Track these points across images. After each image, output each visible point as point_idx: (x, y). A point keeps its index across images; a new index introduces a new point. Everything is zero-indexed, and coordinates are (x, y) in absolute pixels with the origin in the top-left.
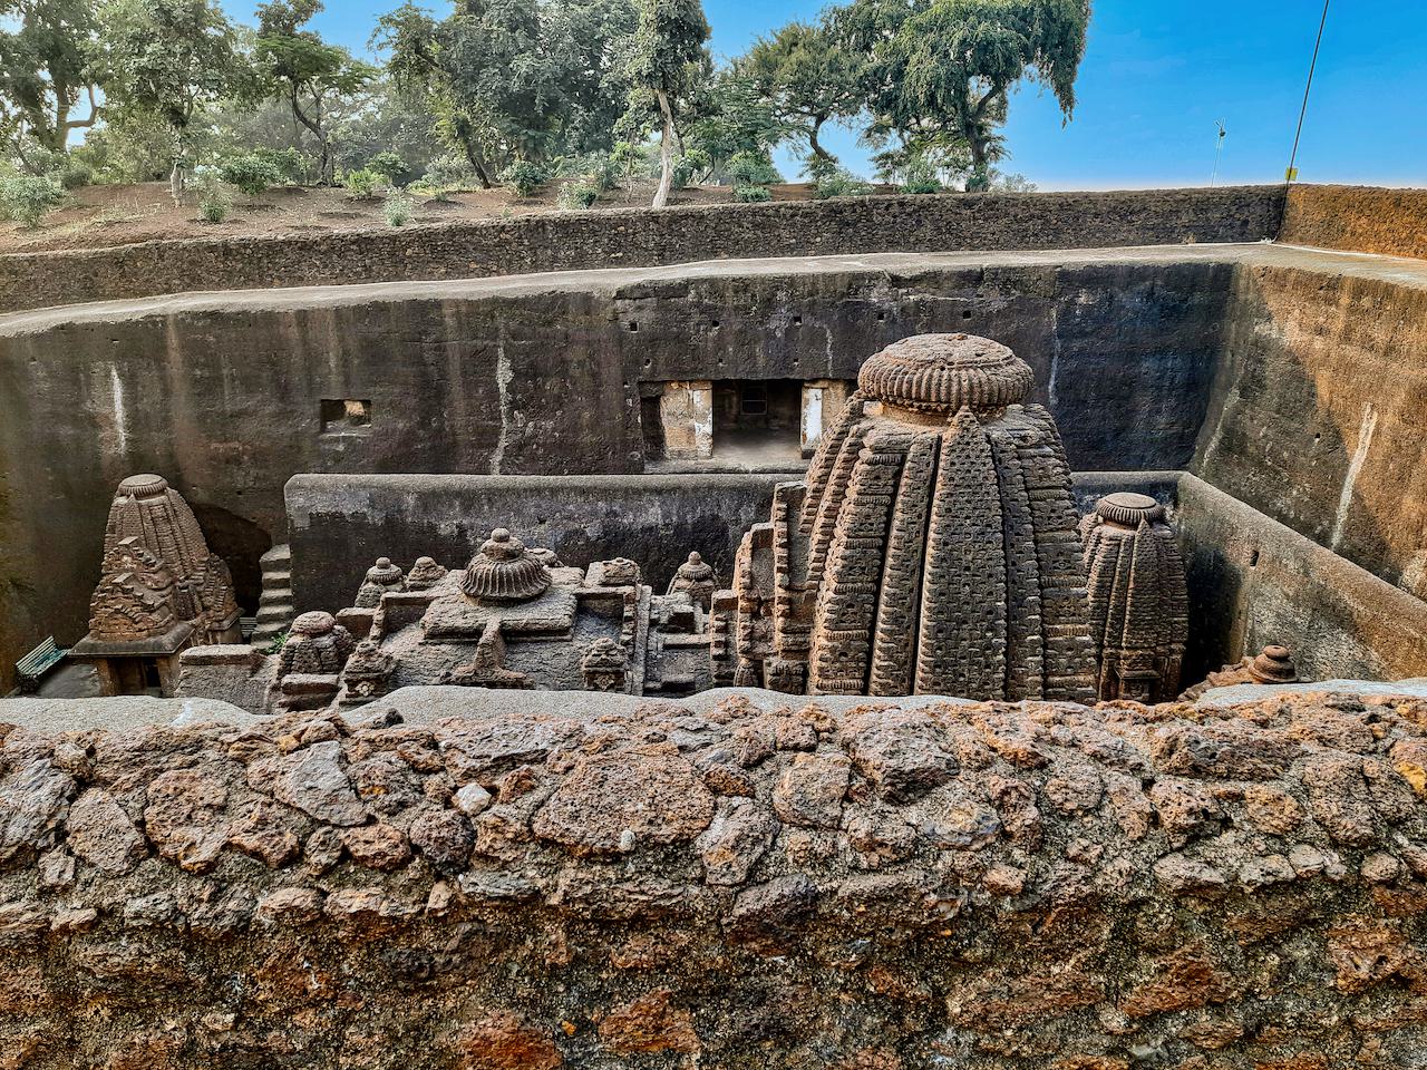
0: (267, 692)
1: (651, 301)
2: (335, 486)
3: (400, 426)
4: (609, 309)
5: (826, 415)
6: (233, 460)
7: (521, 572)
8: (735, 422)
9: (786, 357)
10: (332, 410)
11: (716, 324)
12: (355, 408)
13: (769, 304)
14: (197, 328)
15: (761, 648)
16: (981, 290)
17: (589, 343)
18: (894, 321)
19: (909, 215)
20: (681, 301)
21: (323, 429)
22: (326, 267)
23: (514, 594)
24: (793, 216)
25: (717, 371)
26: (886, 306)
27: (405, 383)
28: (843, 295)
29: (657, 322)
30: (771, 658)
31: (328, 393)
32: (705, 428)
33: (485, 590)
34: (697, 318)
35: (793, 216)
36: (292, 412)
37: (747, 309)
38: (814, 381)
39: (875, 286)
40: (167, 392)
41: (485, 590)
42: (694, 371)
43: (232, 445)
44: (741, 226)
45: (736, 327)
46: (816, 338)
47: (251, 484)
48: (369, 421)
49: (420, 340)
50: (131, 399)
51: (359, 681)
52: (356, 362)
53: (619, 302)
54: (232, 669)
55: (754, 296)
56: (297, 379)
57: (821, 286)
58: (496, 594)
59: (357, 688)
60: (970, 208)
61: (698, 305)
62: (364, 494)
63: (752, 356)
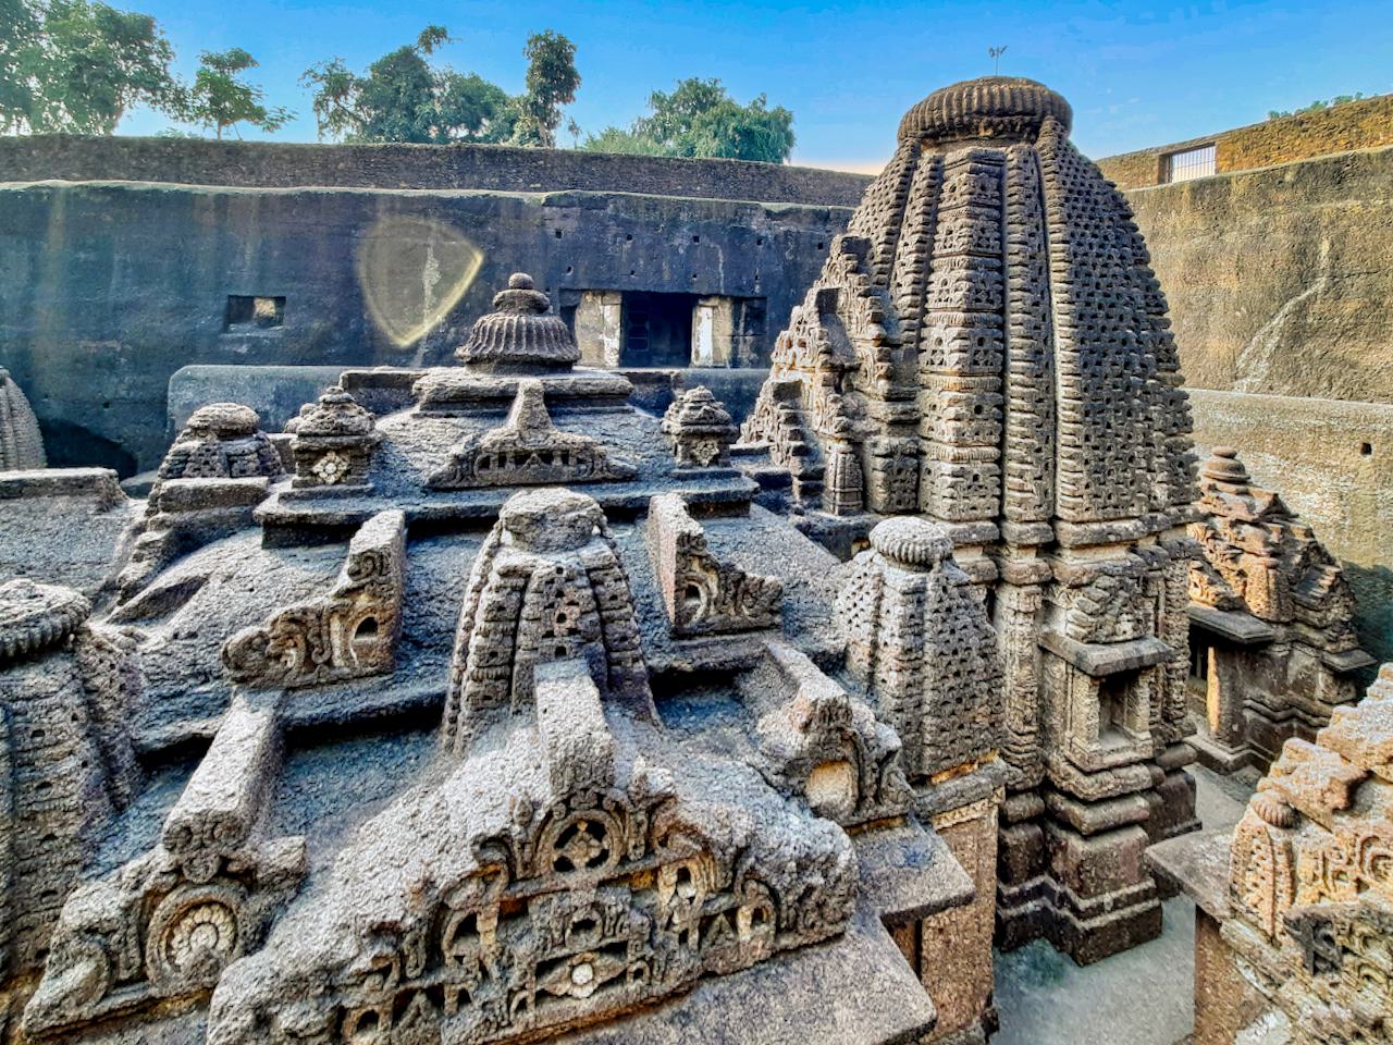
0: (123, 537)
1: (576, 210)
2: (235, 377)
3: (316, 325)
4: (538, 214)
6: (109, 365)
9: (688, 273)
10: (239, 309)
11: (629, 238)
12: (266, 308)
13: (674, 224)
14: (93, 204)
15: (859, 426)
16: (828, 227)
17: (516, 247)
20: (601, 213)
21: (226, 329)
22: (252, 173)
23: (546, 354)
25: (630, 282)
27: (326, 279)
29: (580, 231)
30: (875, 438)
31: (238, 287)
32: (613, 343)
33: (506, 347)
34: (614, 229)
36: (191, 307)
37: (657, 226)
38: (707, 297)
40: (35, 277)
41: (507, 347)
42: (610, 280)
43: (110, 344)
45: (648, 241)
47: (123, 393)
48: (280, 322)
49: (349, 235)
51: (322, 452)
52: (276, 253)
53: (547, 209)
54: (62, 503)
56: (203, 269)
57: (714, 211)
58: (523, 351)
59: (317, 468)
61: (615, 217)
62: (270, 387)
63: (659, 271)
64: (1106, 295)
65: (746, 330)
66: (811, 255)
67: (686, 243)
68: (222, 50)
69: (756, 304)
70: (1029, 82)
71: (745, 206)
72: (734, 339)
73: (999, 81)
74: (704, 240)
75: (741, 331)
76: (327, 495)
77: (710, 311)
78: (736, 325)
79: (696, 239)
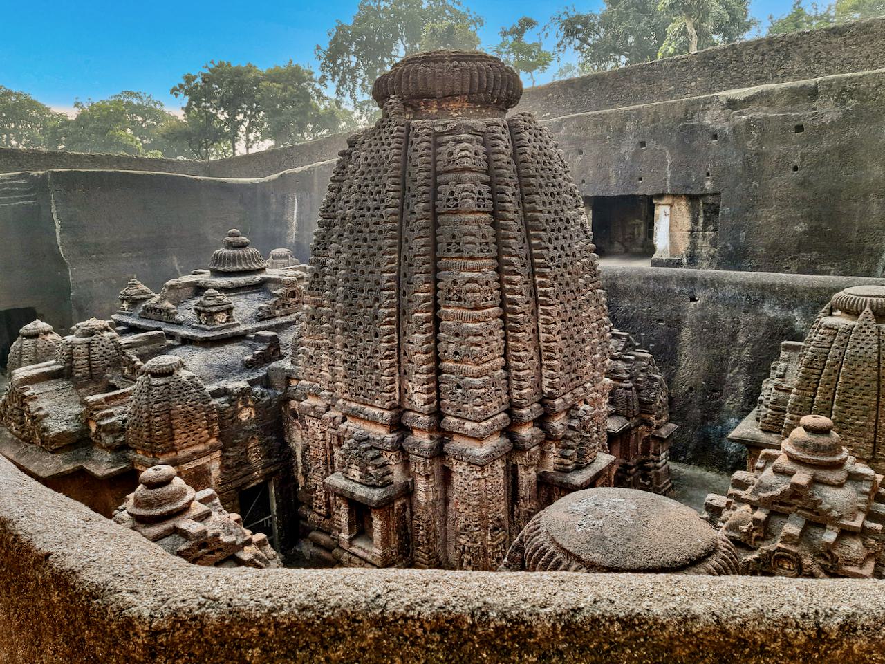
5: (674, 229)
7: (225, 256)
8: (643, 247)
9: (631, 177)
18: (726, 140)
19: (778, 51)
24: (672, 67)
26: (719, 127)
28: (681, 120)
35: (672, 67)
37: (603, 138)
39: (708, 109)
44: (631, 81)
46: (659, 161)
50: (300, 213)
55: (609, 127)
57: (661, 114)
60: (841, 35)
63: (606, 177)
64: (370, 247)
65: (705, 226)
66: (784, 141)
67: (632, 149)
68: (513, 22)
69: (710, 200)
70: (116, 96)
71: (698, 102)
72: (693, 233)
73: (132, 94)
74: (651, 144)
75: (700, 227)
76: (224, 328)
77: (667, 208)
78: (695, 221)
79: (643, 144)
